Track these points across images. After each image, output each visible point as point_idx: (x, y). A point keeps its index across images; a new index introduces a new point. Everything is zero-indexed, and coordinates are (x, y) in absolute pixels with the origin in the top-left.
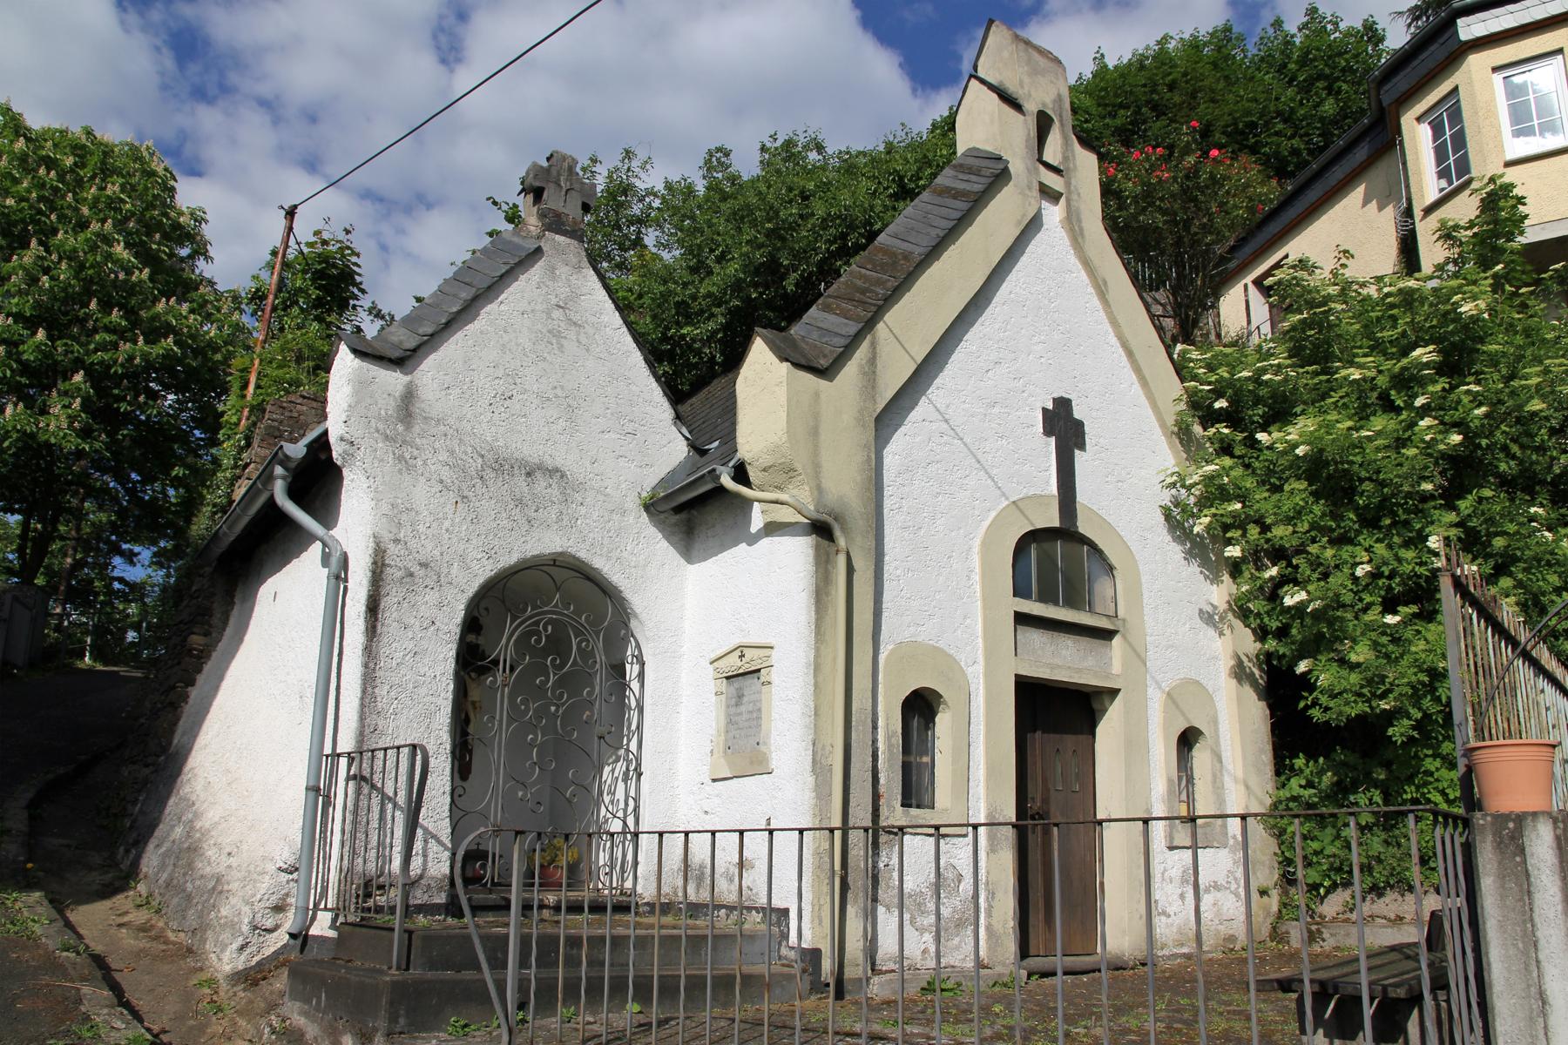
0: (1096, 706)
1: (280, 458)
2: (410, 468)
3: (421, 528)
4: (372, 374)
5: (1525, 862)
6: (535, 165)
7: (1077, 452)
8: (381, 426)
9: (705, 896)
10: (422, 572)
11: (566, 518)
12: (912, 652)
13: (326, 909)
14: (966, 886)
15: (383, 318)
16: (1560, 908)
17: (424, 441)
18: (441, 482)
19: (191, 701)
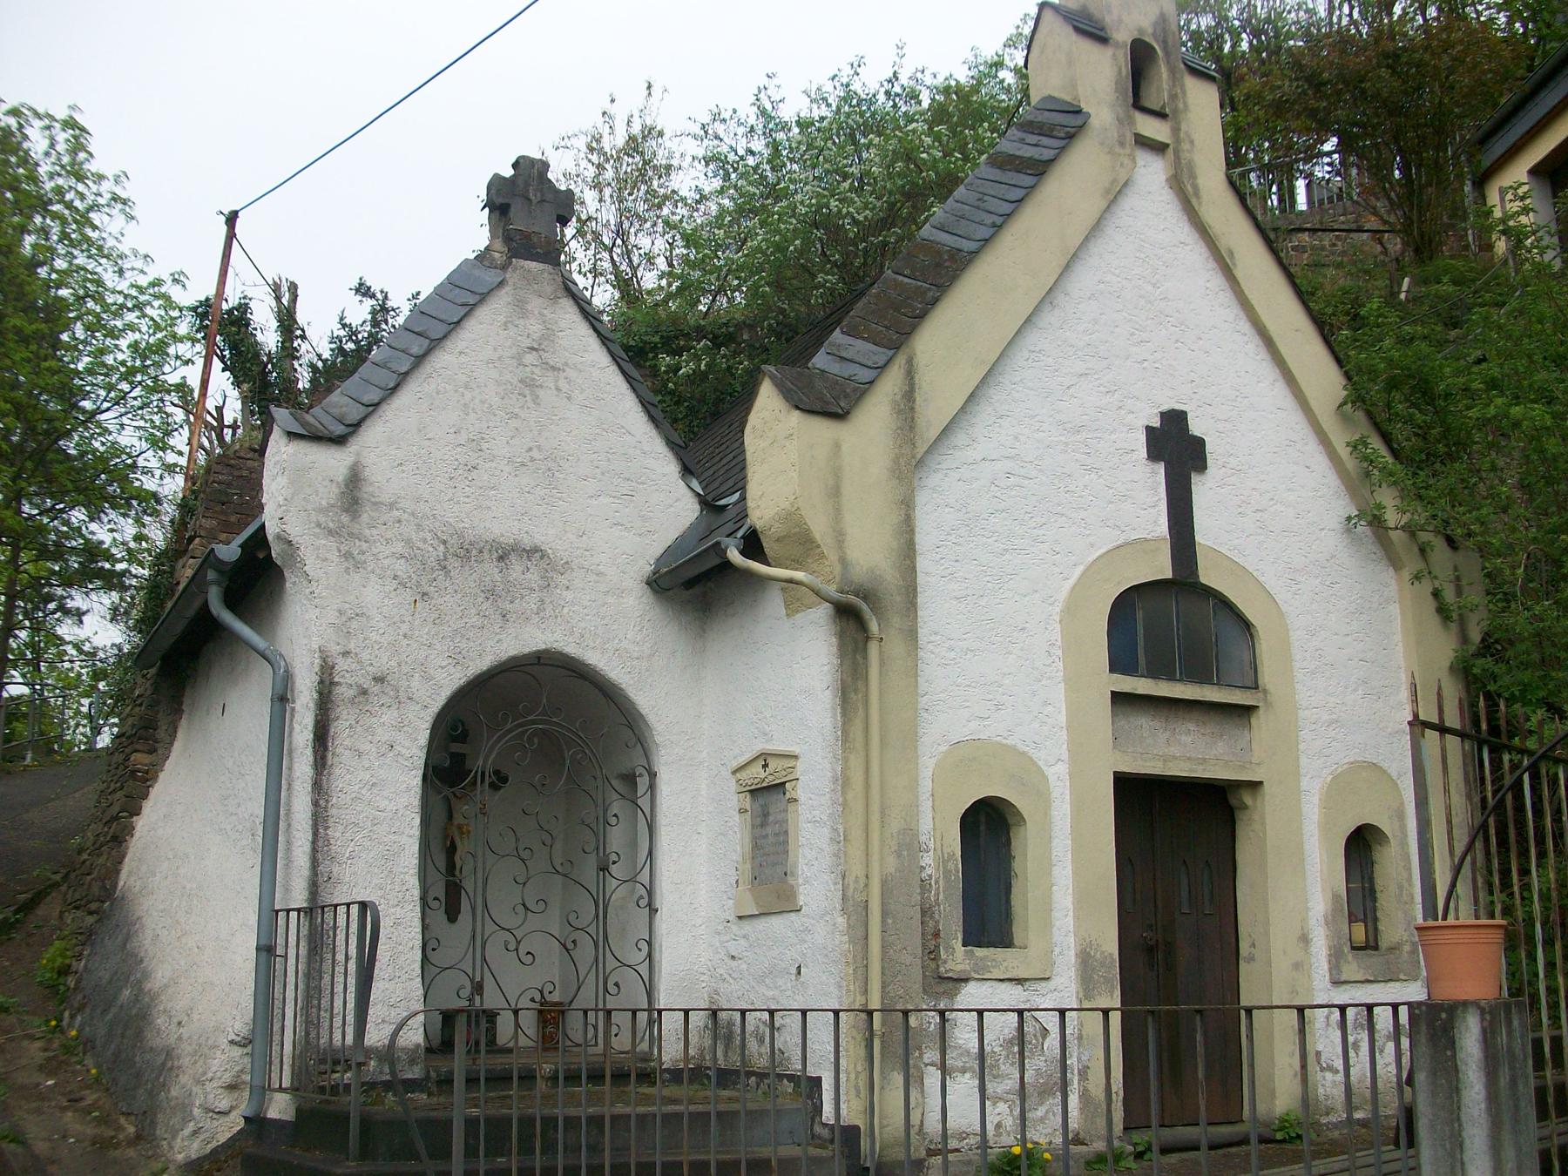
0: (1233, 802)
1: (210, 560)
2: (358, 565)
3: (374, 636)
4: (310, 458)
5: (1454, 1056)
6: (496, 176)
7: (1195, 478)
8: (322, 519)
9: (735, 1061)
10: (377, 689)
11: (549, 609)
12: (967, 754)
13: (281, 1089)
14: (1053, 1041)
15: (373, 296)
16: (1483, 1106)
17: (374, 532)
18: (395, 577)
19: (137, 834)
